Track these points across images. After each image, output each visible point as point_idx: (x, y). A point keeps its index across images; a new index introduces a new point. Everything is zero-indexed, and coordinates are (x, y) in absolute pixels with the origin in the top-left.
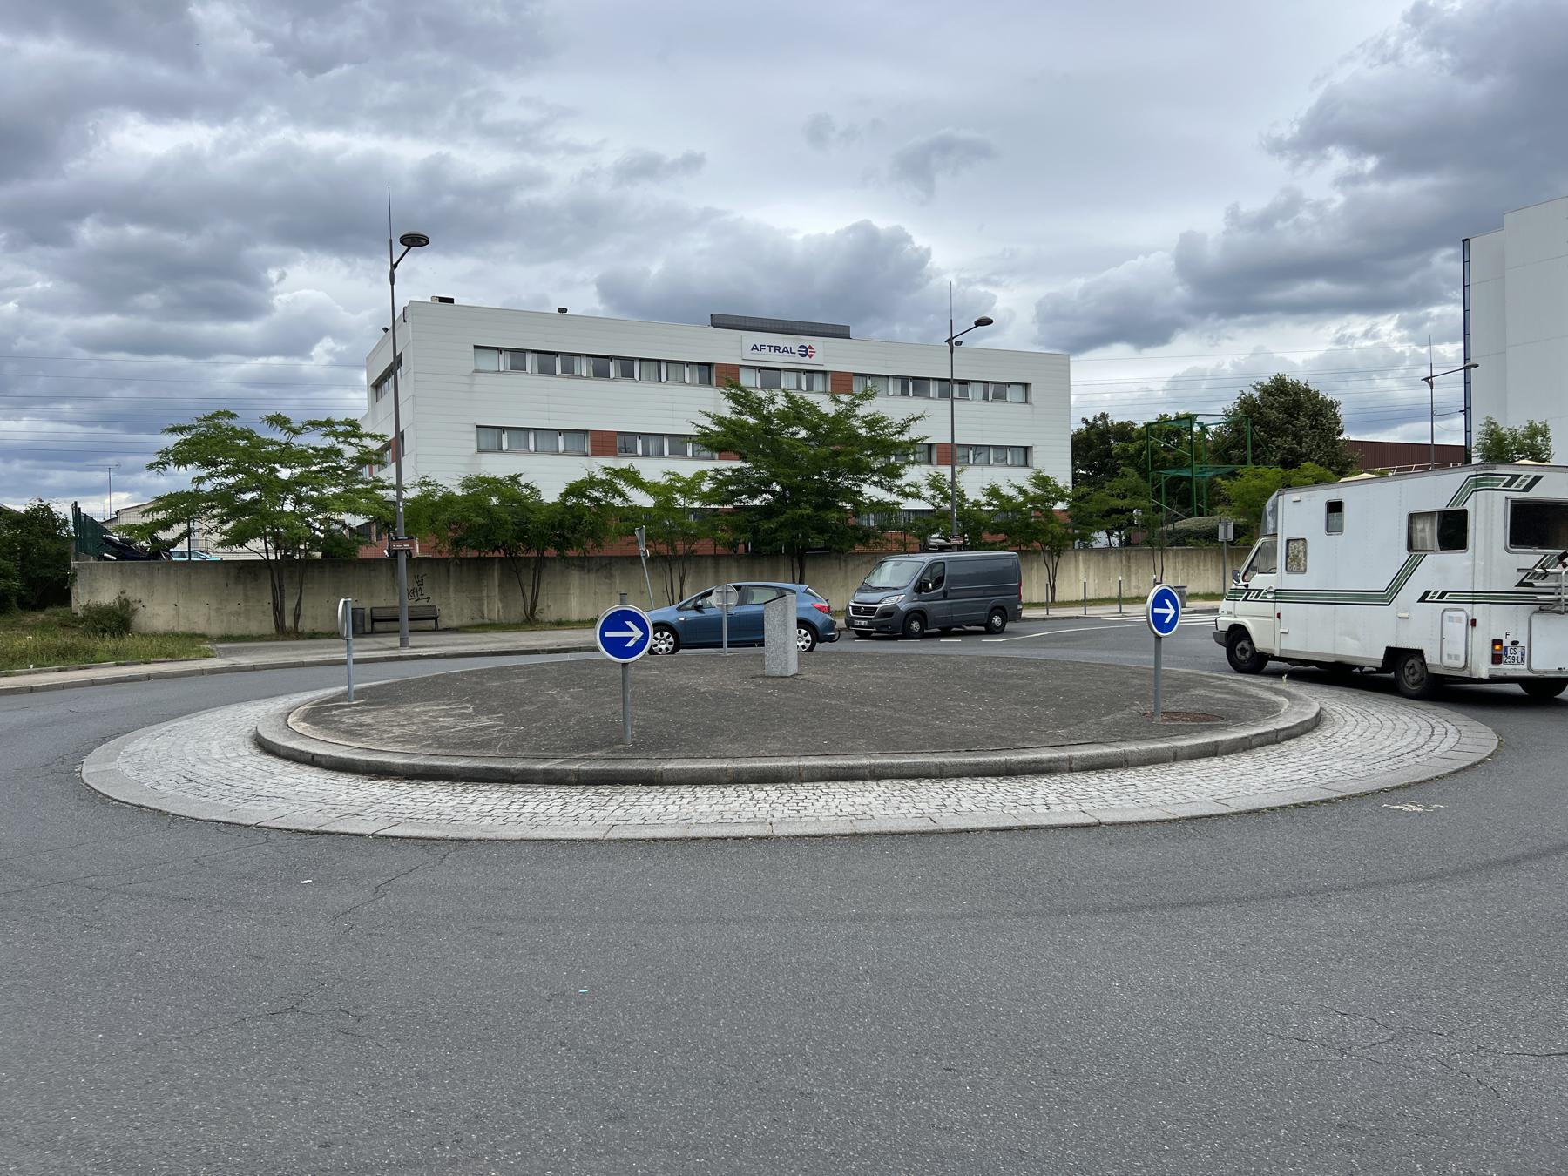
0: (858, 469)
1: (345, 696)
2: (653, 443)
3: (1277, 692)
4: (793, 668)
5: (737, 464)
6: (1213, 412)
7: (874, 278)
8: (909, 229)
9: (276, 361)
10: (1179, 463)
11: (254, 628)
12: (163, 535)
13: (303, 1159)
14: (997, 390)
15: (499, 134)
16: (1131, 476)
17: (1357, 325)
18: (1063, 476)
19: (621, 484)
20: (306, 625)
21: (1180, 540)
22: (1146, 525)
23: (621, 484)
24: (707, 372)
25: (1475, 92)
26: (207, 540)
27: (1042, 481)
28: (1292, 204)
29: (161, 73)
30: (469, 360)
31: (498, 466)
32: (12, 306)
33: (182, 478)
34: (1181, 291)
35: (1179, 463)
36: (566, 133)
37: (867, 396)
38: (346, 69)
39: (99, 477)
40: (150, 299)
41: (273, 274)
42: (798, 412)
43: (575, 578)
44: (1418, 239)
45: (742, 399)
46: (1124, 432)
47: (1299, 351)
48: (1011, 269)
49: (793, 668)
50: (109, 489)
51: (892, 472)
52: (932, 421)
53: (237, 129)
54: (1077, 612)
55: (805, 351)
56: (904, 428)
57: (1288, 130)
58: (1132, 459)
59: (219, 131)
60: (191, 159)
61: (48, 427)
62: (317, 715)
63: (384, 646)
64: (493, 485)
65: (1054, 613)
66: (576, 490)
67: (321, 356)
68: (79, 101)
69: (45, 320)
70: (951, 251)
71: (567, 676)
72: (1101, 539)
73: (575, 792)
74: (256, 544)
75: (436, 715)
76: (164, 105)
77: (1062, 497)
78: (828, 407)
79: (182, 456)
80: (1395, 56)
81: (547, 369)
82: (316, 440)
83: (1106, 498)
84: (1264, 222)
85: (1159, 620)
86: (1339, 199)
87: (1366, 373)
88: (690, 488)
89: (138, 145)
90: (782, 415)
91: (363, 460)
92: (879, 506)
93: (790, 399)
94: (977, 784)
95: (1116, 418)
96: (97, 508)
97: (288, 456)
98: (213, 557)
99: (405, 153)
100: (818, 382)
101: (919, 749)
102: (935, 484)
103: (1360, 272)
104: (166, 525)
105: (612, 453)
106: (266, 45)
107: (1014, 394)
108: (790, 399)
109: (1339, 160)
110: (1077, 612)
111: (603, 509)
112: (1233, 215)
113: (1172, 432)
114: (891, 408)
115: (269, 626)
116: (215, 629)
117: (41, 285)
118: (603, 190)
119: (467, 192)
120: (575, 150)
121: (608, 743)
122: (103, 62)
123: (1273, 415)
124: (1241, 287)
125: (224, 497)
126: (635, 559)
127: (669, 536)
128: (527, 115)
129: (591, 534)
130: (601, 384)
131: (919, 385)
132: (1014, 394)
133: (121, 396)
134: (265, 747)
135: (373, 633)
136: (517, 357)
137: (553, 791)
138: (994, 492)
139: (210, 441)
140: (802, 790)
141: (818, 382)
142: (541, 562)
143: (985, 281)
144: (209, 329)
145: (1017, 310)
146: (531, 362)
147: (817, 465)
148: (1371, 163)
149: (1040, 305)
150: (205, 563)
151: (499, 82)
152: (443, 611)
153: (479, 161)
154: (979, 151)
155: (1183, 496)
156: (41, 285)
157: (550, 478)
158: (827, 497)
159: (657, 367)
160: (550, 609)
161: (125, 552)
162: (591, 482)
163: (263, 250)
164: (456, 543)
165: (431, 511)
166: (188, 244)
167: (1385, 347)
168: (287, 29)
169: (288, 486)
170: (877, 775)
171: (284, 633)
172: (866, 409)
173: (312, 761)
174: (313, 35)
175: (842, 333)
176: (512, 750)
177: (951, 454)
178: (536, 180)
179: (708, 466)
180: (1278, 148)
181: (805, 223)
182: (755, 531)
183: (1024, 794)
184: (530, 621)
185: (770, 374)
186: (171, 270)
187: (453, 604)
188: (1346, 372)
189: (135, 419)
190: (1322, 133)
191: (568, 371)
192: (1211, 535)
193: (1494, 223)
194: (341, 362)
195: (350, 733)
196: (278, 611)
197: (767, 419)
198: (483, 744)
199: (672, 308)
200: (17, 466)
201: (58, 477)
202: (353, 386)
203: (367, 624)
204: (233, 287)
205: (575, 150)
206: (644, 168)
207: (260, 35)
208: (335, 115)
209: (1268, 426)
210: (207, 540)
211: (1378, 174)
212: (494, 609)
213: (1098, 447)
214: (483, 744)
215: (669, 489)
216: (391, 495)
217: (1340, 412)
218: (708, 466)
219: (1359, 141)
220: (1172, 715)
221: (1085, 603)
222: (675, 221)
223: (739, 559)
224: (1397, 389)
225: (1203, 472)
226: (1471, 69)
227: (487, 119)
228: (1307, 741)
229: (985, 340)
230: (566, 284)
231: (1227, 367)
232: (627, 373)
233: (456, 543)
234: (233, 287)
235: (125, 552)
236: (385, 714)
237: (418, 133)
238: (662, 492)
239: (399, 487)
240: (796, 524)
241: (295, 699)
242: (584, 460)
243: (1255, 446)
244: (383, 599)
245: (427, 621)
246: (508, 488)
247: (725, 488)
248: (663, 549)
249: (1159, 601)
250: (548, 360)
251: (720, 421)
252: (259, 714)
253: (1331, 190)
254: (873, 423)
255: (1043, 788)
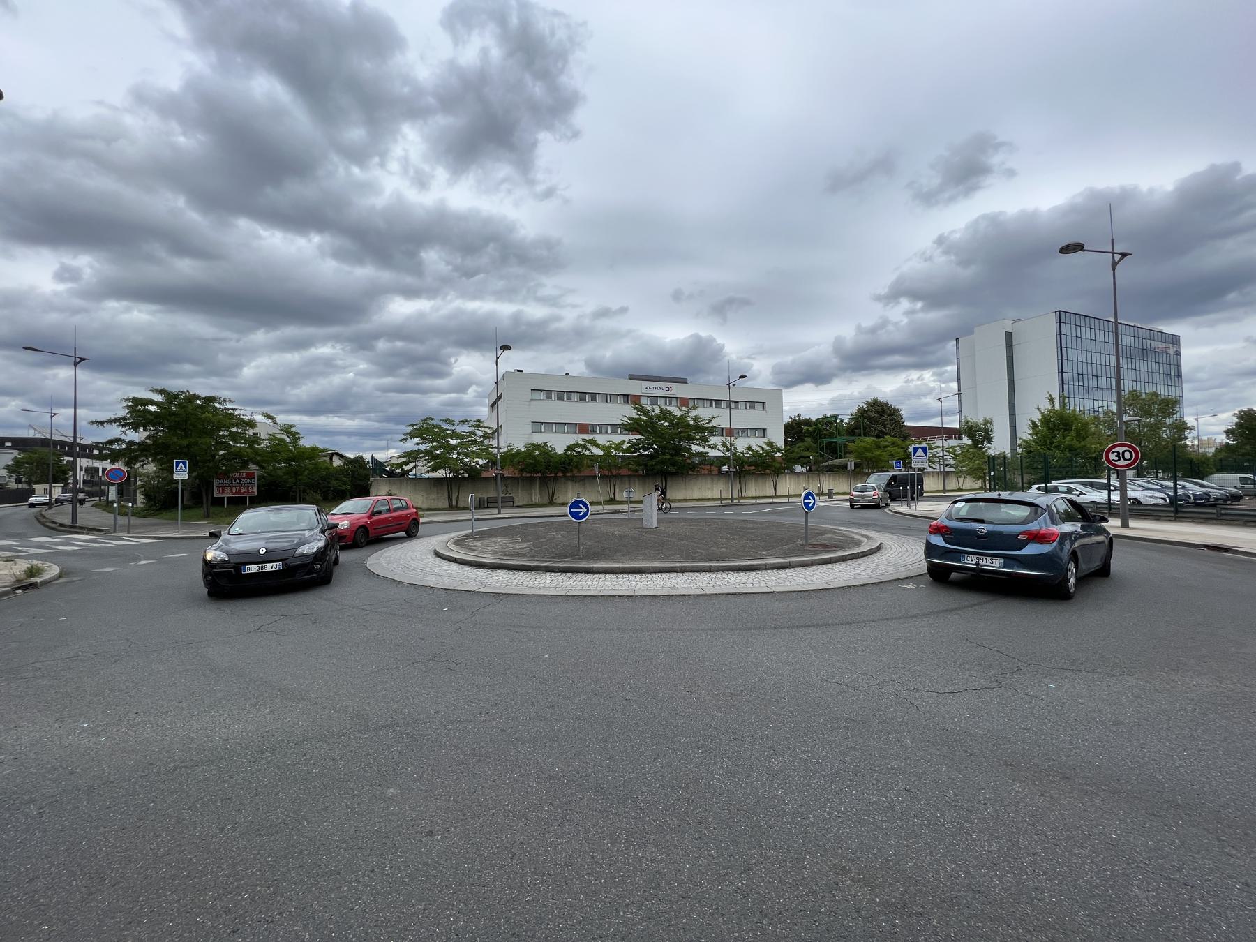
0: (690, 439)
1: (471, 534)
2: (604, 429)
3: (863, 536)
4: (655, 525)
5: (639, 437)
6: (846, 415)
7: (700, 357)
8: (715, 336)
9: (453, 395)
10: (831, 436)
11: (440, 505)
12: (406, 468)
13: (427, 717)
14: (751, 405)
15: (543, 300)
16: (808, 440)
17: (914, 374)
18: (780, 442)
19: (589, 446)
20: (461, 504)
21: (831, 469)
22: (816, 463)
23: (589, 446)
24: (626, 398)
25: (968, 274)
26: (421, 469)
27: (770, 444)
28: (884, 323)
29: (409, 280)
30: (529, 395)
31: (539, 439)
32: (351, 374)
33: (411, 445)
34: (835, 361)
35: (831, 436)
36: (570, 299)
37: (695, 408)
38: (482, 275)
39: (384, 443)
40: (405, 371)
41: (453, 360)
42: (664, 415)
43: (570, 485)
44: (941, 338)
45: (640, 409)
46: (808, 422)
47: (886, 387)
48: (760, 352)
49: (655, 525)
50: (388, 448)
51: (705, 440)
52: (721, 418)
53: (438, 302)
54: (786, 500)
55: (668, 389)
56: (710, 421)
57: (883, 291)
58: (810, 434)
59: (432, 302)
60: (421, 315)
61: (365, 423)
62: (459, 542)
63: (492, 513)
64: (537, 447)
65: (775, 500)
66: (570, 448)
67: (472, 392)
68: (376, 293)
69: (363, 380)
70: (733, 345)
71: (560, 527)
72: (798, 468)
73: (557, 575)
74: (442, 471)
75: (506, 543)
76: (410, 293)
77: (779, 450)
78: (677, 413)
79: (412, 435)
80: (930, 259)
81: (560, 398)
82: (465, 429)
83: (799, 449)
84: (873, 331)
85: (807, 505)
86: (905, 320)
87: (919, 395)
88: (618, 447)
89: (401, 309)
90: (658, 417)
91: (485, 437)
92: (701, 454)
93: (662, 410)
94: (725, 575)
95: (803, 417)
96: (382, 456)
97: (454, 435)
98: (427, 476)
99: (505, 309)
100: (674, 402)
101: (702, 560)
102: (724, 445)
103: (916, 352)
104: (406, 463)
105: (586, 432)
106: (450, 267)
107: (759, 406)
108: (662, 410)
109: (905, 304)
110: (786, 500)
111: (581, 456)
112: (859, 328)
113: (829, 422)
114: (704, 413)
115: (446, 505)
116: (425, 506)
117: (363, 366)
118: (586, 322)
119: (531, 324)
120: (574, 306)
121: (572, 555)
122: (386, 276)
123: (873, 415)
124: (861, 359)
125: (428, 452)
126: (594, 477)
127: (609, 467)
128: (555, 292)
129: (576, 467)
130: (583, 404)
131: (718, 403)
132: (759, 406)
133: (393, 410)
134: (438, 555)
135: (488, 508)
136: (548, 393)
137: (548, 575)
138: (749, 448)
139: (425, 430)
140: (651, 577)
141: (674, 402)
142: (556, 478)
143: (749, 357)
144: (428, 382)
145: (762, 371)
146: (554, 395)
147: (672, 437)
148: (919, 305)
149: (774, 367)
150: (423, 479)
151: (544, 280)
152: (516, 499)
153: (535, 312)
154: (745, 302)
155: (834, 450)
156: (363, 366)
157: (559, 443)
158: (678, 450)
159: (606, 397)
160: (559, 498)
161: (391, 474)
162: (577, 445)
163: (449, 350)
164: (522, 470)
165: (511, 458)
166: (419, 349)
167: (926, 385)
168: (459, 261)
169: (454, 448)
170: (683, 570)
171: (452, 508)
172: (693, 413)
173: (455, 561)
174: (470, 262)
175: (684, 381)
176: (533, 558)
177: (731, 432)
178: (558, 319)
179: (626, 438)
180: (878, 298)
181: (671, 333)
182: (646, 465)
183: (744, 579)
184: (551, 503)
185: (653, 399)
186: (410, 359)
187: (520, 496)
188: (909, 396)
189: (397, 420)
190: (896, 293)
191: (569, 398)
192: (845, 467)
193: (969, 331)
194: (480, 396)
195: (472, 549)
196: (450, 499)
197: (651, 417)
198: (521, 555)
199: (616, 371)
200: (353, 439)
201: (368, 443)
202: (483, 405)
203: (482, 505)
204: (436, 366)
205: (574, 306)
206: (604, 313)
207: (448, 263)
208: (477, 295)
209: (869, 418)
210: (421, 469)
211: (922, 310)
212: (537, 498)
213: (796, 429)
214: (521, 555)
215: (609, 447)
216: (495, 451)
217: (902, 413)
218: (626, 438)
219: (914, 295)
220: (814, 546)
221: (789, 496)
222: (615, 335)
223: (639, 476)
224: (931, 402)
225: (841, 440)
226: (965, 263)
227: (539, 294)
228: (878, 555)
229: (747, 384)
230: (571, 362)
231: (856, 393)
232: (593, 399)
233: (522, 470)
234: (436, 366)
235: (391, 474)
236: (486, 542)
237: (511, 301)
238: (607, 450)
239: (498, 448)
240: (663, 462)
241: (453, 535)
242: (575, 436)
243: (865, 428)
244: (492, 494)
245: (509, 503)
246: (543, 449)
247: (634, 446)
248: (607, 473)
249: (807, 497)
250: (560, 395)
251: (631, 419)
252: (436, 542)
253: (901, 317)
254: (696, 419)
255: (753, 577)
